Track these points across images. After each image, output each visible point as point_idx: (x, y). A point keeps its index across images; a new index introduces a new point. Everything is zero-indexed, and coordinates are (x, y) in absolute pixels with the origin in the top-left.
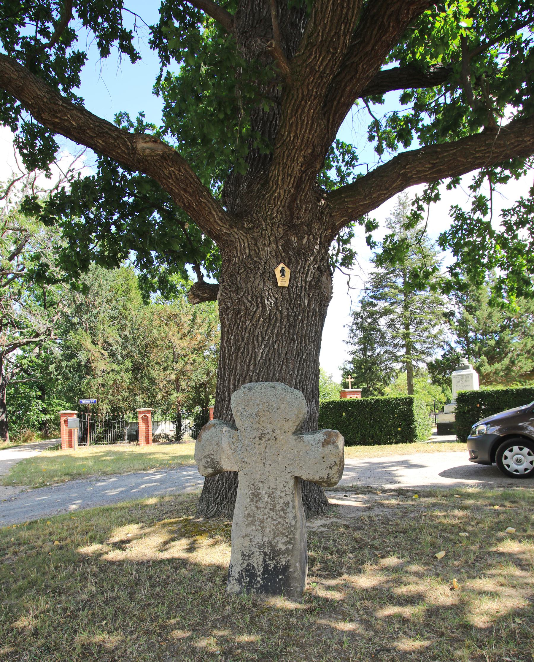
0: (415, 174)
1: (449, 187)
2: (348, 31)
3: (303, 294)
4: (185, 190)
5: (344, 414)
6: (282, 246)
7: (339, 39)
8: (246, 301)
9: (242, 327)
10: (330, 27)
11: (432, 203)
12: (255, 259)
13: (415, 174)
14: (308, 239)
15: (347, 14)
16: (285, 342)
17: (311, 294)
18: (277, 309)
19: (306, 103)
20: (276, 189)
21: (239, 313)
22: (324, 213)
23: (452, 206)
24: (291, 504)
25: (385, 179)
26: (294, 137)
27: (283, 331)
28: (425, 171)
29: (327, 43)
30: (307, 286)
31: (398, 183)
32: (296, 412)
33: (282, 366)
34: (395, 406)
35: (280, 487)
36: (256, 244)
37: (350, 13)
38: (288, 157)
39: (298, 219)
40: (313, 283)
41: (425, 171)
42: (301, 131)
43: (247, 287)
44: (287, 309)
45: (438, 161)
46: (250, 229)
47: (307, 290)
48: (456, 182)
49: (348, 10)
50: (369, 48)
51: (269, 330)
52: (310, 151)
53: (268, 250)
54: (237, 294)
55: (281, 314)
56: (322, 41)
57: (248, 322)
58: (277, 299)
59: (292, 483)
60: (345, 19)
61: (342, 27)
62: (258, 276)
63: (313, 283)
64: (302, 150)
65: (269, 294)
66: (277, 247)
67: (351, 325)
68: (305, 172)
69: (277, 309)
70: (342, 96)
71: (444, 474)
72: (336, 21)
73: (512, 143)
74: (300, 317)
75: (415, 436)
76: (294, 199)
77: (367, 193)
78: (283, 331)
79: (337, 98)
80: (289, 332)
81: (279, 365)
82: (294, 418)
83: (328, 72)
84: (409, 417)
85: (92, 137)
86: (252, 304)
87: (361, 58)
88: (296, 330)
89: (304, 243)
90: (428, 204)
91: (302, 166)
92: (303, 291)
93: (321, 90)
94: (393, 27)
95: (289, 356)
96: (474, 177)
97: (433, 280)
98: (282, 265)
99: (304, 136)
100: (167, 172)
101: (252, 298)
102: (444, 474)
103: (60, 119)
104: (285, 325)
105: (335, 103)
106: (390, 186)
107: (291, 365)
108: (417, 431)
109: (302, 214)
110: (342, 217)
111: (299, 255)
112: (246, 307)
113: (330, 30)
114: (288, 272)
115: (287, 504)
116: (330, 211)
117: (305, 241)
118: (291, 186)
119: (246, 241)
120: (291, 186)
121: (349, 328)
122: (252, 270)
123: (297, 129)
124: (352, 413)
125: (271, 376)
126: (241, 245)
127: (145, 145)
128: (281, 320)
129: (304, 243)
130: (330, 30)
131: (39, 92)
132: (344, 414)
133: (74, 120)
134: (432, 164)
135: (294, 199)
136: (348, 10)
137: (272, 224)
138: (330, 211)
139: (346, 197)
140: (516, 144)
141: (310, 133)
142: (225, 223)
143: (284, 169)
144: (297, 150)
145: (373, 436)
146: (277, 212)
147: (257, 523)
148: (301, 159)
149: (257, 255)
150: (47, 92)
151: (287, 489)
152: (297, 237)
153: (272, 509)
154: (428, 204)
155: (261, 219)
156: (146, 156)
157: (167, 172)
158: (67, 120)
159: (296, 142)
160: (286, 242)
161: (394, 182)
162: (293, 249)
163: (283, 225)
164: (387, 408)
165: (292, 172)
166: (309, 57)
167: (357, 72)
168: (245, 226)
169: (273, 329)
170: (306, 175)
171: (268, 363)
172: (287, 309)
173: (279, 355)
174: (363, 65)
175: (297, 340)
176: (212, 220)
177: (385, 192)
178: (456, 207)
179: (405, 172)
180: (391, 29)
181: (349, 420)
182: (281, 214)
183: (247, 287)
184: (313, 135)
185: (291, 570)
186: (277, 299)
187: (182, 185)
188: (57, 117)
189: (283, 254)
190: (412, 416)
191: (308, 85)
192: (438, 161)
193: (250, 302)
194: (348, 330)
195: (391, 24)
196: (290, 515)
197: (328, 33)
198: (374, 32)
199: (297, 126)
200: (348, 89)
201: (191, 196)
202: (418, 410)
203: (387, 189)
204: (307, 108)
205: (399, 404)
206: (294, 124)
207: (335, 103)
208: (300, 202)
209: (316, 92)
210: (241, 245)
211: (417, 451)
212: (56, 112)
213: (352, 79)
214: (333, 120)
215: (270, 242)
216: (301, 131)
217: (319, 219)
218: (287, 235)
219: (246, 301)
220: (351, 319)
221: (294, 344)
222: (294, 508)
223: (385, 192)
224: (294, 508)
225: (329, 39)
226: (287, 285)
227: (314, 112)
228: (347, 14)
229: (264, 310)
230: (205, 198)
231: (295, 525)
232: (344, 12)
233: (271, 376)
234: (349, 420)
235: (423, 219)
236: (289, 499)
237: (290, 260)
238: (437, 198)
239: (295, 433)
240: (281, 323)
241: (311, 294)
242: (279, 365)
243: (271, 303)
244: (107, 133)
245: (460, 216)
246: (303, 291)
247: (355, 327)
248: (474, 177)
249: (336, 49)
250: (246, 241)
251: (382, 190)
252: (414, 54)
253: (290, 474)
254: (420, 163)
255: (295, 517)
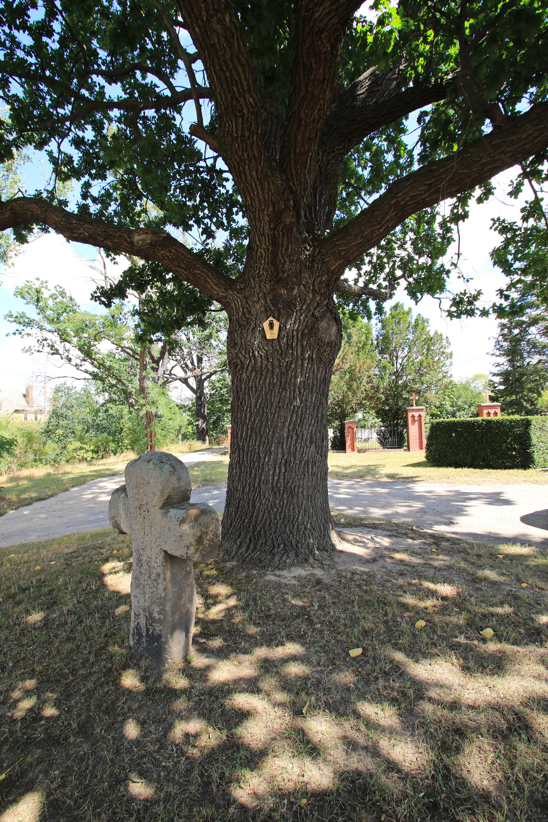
0: (409, 201)
1: (480, 200)
2: (244, 91)
3: (294, 344)
4: (179, 267)
5: (454, 435)
6: (270, 300)
7: (238, 101)
8: (241, 356)
9: (240, 379)
10: (225, 93)
11: (460, 223)
12: (247, 316)
13: (409, 201)
14: (298, 289)
15: (231, 76)
16: (277, 391)
17: (305, 343)
18: (268, 360)
19: (244, 168)
20: (258, 249)
21: (237, 366)
22: (315, 261)
23: (493, 219)
24: (162, 576)
25: (376, 213)
26: (251, 200)
27: (275, 381)
28: (421, 195)
29: (231, 109)
30: (299, 335)
31: (392, 213)
32: (161, 488)
33: (274, 414)
34: (509, 428)
35: (153, 557)
36: (247, 303)
37: (234, 73)
38: (255, 219)
39: (284, 272)
40: (306, 331)
41: (421, 195)
42: (254, 194)
43: (241, 343)
44: (279, 360)
45: (433, 180)
46: (242, 289)
47: (299, 339)
48: (488, 192)
49: (231, 72)
50: (303, 93)
51: (261, 382)
52: (271, 209)
53: (258, 306)
54: (235, 349)
55: (272, 365)
56: (225, 109)
57: (244, 374)
58: (267, 351)
59: (161, 557)
60: (232, 81)
61: (235, 89)
62: (250, 331)
63: (306, 331)
64: (264, 210)
65: (259, 347)
66: (266, 302)
67: (497, 336)
68: (274, 229)
69: (268, 360)
70: (296, 147)
71: (527, 519)
72: (225, 86)
73: (530, 135)
74: (293, 366)
75: (533, 462)
76: (275, 255)
77: (357, 232)
78: (275, 381)
79: (292, 150)
80: (281, 381)
81: (272, 413)
82: (159, 493)
83: (247, 134)
84: (526, 440)
85: (102, 241)
86: (246, 358)
87: (299, 104)
88: (289, 379)
89: (294, 294)
90: (457, 224)
91: (270, 225)
92: (295, 340)
93: (253, 151)
94: (316, 63)
95: (281, 404)
96: (512, 181)
97: (479, 304)
98: (271, 318)
99: (259, 197)
100: (160, 255)
101: (245, 352)
102: (527, 519)
103: (77, 233)
104: (277, 375)
105: (292, 155)
106: (383, 219)
107: (282, 414)
108: (535, 457)
109: (286, 267)
110: (336, 261)
111: (289, 307)
112: (241, 361)
113: (226, 97)
114: (276, 324)
115: (158, 575)
116: (323, 257)
117: (295, 291)
118: (267, 244)
119: (239, 300)
120: (267, 244)
121: (495, 340)
122: (245, 327)
123: (250, 194)
124: (462, 434)
125: (264, 424)
126: (235, 305)
127: (139, 238)
128: (273, 370)
129: (294, 294)
130: (226, 97)
131: (56, 219)
132: (454, 435)
133: (87, 232)
134: (428, 184)
135: (275, 255)
136: (231, 72)
137: (260, 281)
138: (323, 257)
139: (338, 240)
140: (536, 134)
141: (263, 193)
142: (220, 288)
143: (256, 230)
144: (259, 210)
145: (484, 458)
146: (264, 270)
147: (141, 587)
148: (267, 219)
149: (249, 313)
150: (63, 217)
151: (158, 560)
152: (286, 289)
153: (149, 577)
154: (457, 224)
155: (251, 278)
156: (140, 246)
157: (160, 255)
158: (82, 233)
159: (254, 204)
160: (274, 296)
161: (387, 214)
162: (283, 302)
163: (270, 281)
164: (500, 430)
165: (264, 232)
166: (225, 127)
167: (301, 119)
168: (238, 287)
169: (265, 380)
170: (278, 231)
171: (261, 412)
172: (279, 360)
173: (272, 404)
174: (304, 111)
175: (290, 388)
176: (209, 287)
177: (378, 227)
178: (499, 219)
179: (397, 202)
180: (314, 66)
181: (458, 441)
182: (267, 271)
183: (241, 343)
184: (268, 194)
185: (163, 640)
186: (267, 351)
187: (176, 263)
188: (75, 233)
189: (272, 308)
190: (529, 439)
191: (236, 151)
192: (433, 180)
193: (244, 356)
194: (493, 342)
195: (313, 61)
196: (161, 587)
197: (225, 100)
198: (301, 75)
199: (248, 190)
200: (299, 138)
201: (185, 270)
202: (538, 433)
203: (380, 223)
204: (248, 172)
205: (513, 427)
206: (245, 189)
207: (292, 155)
208: (283, 257)
209: (248, 155)
210: (235, 305)
211: (525, 481)
212: (72, 229)
213: (299, 127)
214: (297, 172)
215: (259, 298)
216: (254, 194)
217: (310, 268)
218: (275, 289)
219: (241, 356)
220: (498, 331)
221: (286, 393)
222: (164, 579)
223: (378, 227)
224: (164, 579)
225: (230, 105)
226: (276, 337)
227: (257, 174)
228: (231, 76)
229: (255, 363)
230: (199, 270)
231: (165, 597)
232: (228, 74)
233: (264, 424)
234: (458, 441)
235: (454, 241)
236: (160, 570)
237: (279, 312)
238: (465, 216)
239: (162, 508)
240: (273, 373)
241: (305, 343)
242: (272, 413)
243: (261, 356)
244: (112, 235)
245: (504, 228)
246: (295, 340)
247: (500, 338)
248: (512, 181)
249: (241, 111)
250: (239, 300)
251: (374, 226)
252: (415, 68)
253: (159, 547)
254: (412, 188)
255: (165, 589)
